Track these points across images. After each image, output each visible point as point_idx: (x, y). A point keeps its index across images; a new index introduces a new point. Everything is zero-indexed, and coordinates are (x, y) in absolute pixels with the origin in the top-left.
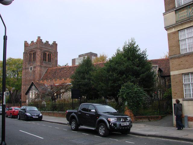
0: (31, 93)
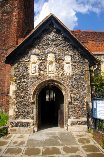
0: (33, 58)
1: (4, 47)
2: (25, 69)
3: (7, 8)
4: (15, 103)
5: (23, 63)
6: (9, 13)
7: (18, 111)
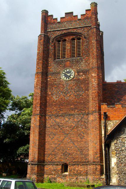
1: (84, 112)
2: (123, 144)
3: (82, 66)
4: (117, 173)
5: (121, 139)
6: (85, 72)
7: (120, 180)
